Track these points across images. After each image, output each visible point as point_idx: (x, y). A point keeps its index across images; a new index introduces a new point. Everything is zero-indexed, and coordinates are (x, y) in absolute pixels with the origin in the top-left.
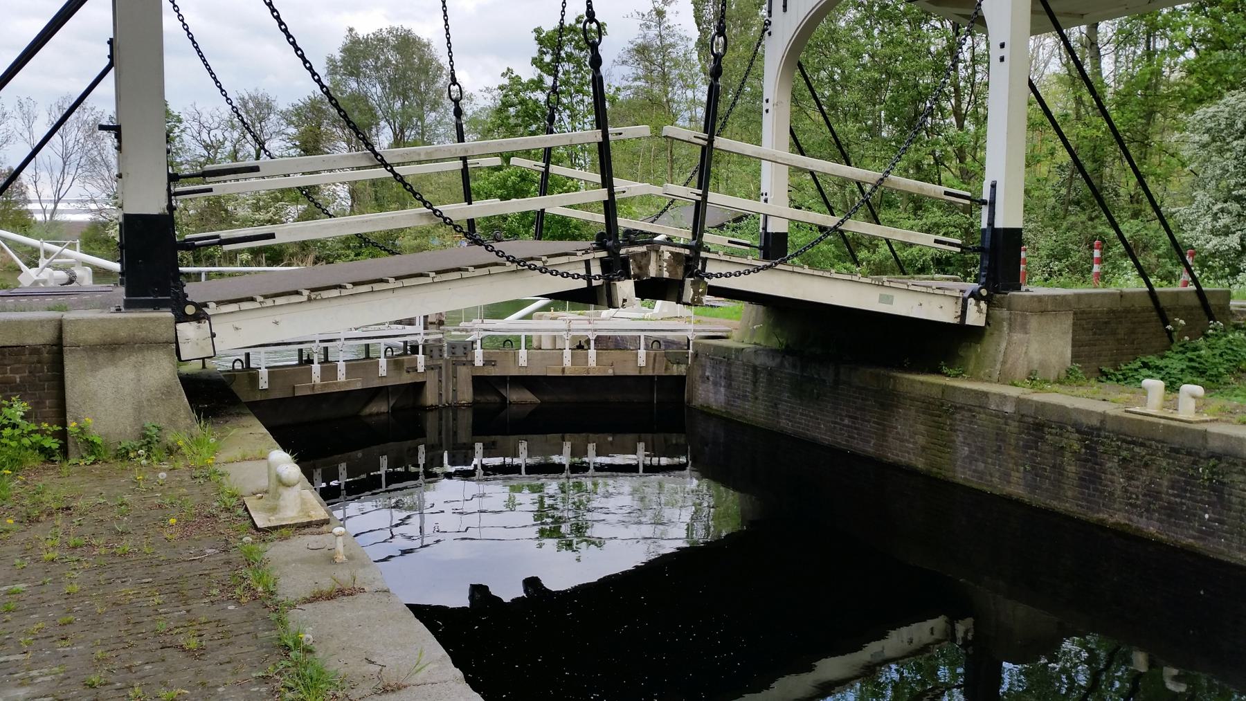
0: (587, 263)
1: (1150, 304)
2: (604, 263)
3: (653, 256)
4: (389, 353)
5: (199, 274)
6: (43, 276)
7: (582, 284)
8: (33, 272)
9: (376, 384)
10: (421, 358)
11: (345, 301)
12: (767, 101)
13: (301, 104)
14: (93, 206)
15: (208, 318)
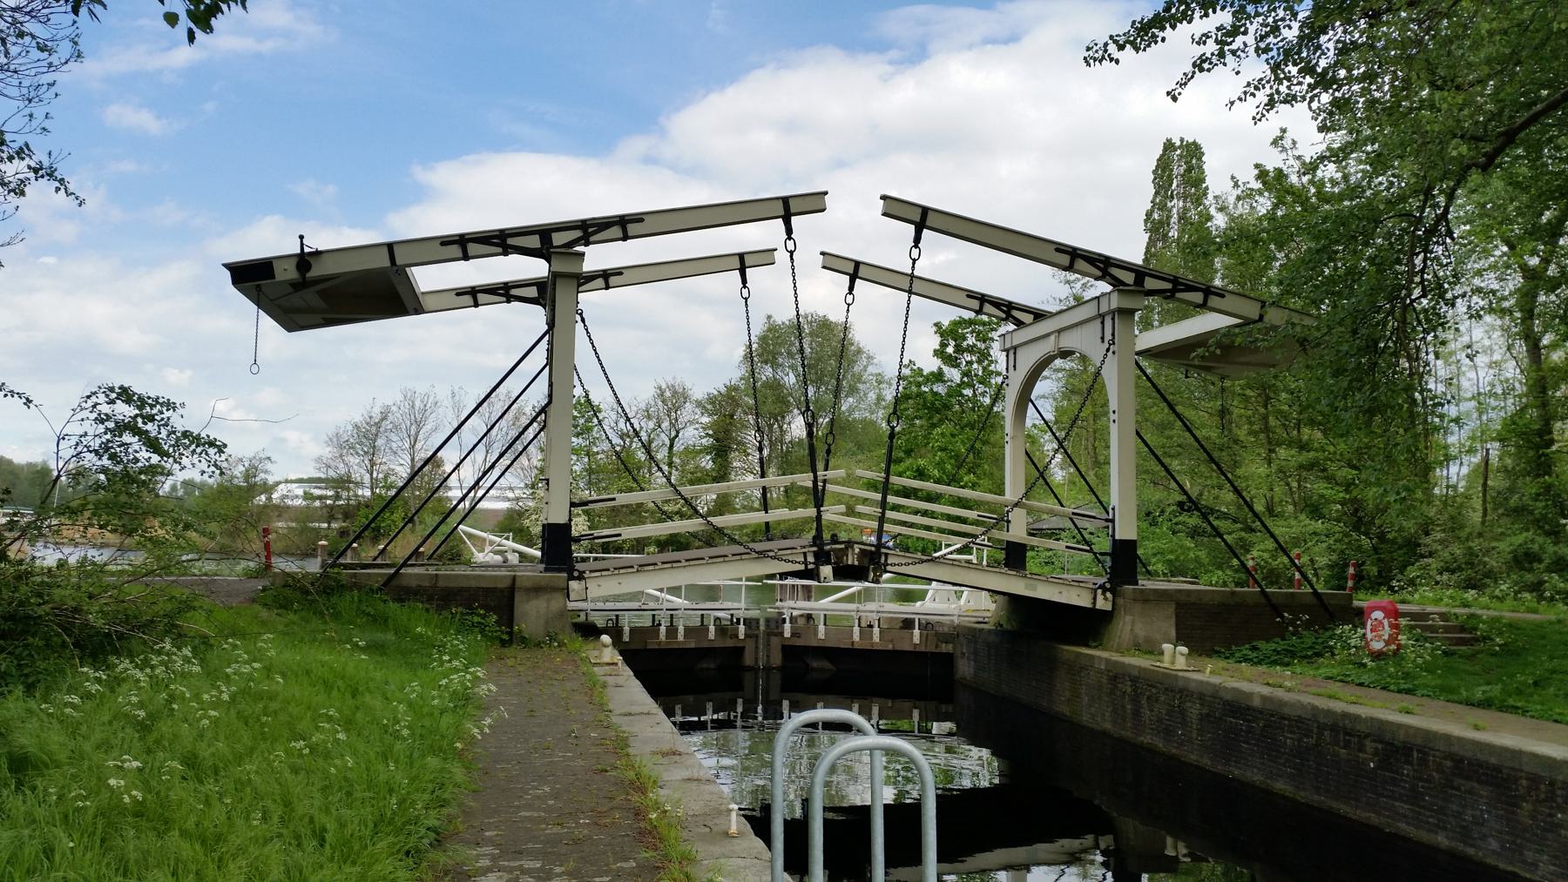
0: (805, 554)
1: (1263, 601)
2: (816, 555)
3: (850, 550)
4: (718, 623)
5: (589, 558)
6: (487, 559)
7: (802, 567)
8: (481, 555)
9: (705, 645)
10: (742, 628)
11: (656, 572)
12: (1114, 412)
13: (716, 393)
14: (511, 495)
15: (584, 578)
